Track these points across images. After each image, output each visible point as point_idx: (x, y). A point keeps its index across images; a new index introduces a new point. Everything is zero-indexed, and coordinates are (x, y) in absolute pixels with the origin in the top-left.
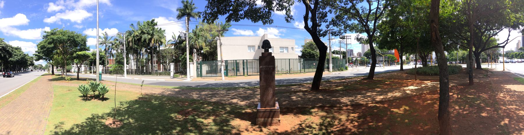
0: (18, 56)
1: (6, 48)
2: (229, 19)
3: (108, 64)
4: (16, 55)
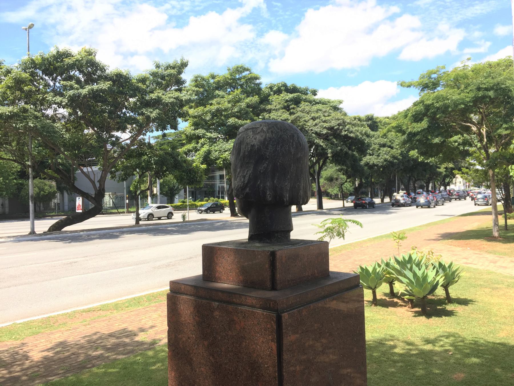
0: (392, 148)
4: (384, 146)
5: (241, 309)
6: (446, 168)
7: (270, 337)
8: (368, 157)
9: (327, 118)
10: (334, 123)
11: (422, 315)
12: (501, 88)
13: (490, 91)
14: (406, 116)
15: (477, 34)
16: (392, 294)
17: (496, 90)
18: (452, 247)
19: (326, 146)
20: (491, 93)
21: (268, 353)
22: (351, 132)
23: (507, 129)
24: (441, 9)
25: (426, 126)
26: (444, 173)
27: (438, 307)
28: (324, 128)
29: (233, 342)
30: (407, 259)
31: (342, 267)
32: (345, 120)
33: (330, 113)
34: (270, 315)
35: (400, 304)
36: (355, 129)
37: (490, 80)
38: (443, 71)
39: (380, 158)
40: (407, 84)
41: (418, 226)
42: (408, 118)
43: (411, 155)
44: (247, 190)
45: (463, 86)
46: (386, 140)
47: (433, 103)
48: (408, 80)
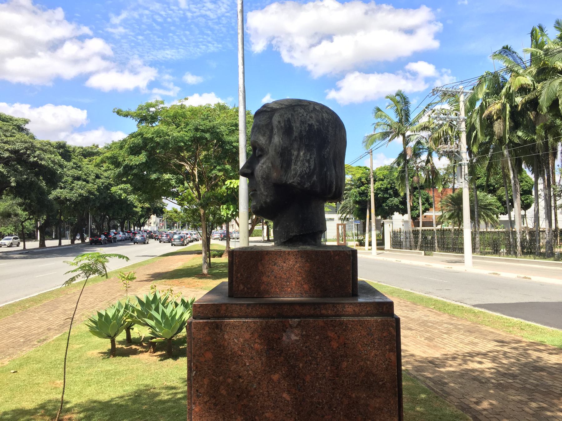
0: (88, 182)
1: (29, 156)
2: (158, 394)
3: (426, 210)
4: (78, 178)
5: (339, 321)
6: (142, 208)
7: (387, 346)
8: (59, 190)
9: (9, 139)
10: (18, 146)
11: (168, 358)
12: (216, 132)
13: (206, 133)
14: (121, 148)
15: (167, 77)
16: (129, 340)
17: (212, 133)
18: (167, 286)
19: (8, 172)
20: (207, 135)
21: (385, 366)
22: (41, 160)
23: (220, 171)
24: (133, 44)
25: (144, 160)
26: (140, 213)
27: (181, 347)
28: (5, 150)
29: (326, 366)
30: (151, 298)
31: (51, 319)
32: (34, 144)
33: (14, 133)
34: (387, 321)
35: (139, 350)
36: (48, 156)
37: (207, 122)
38: (162, 106)
39: (73, 192)
40: (124, 113)
41: (123, 268)
42: (124, 149)
43: (113, 191)
44: (315, 178)
45: (183, 125)
46: (80, 172)
47: (153, 137)
48: (125, 109)
